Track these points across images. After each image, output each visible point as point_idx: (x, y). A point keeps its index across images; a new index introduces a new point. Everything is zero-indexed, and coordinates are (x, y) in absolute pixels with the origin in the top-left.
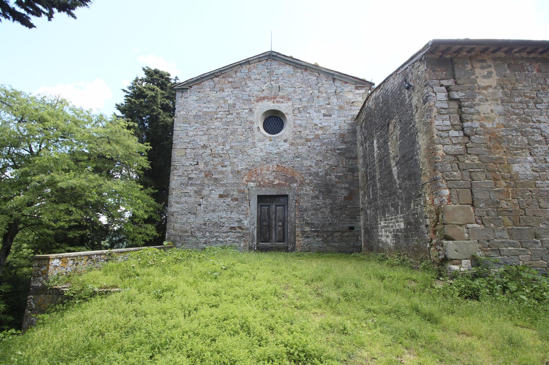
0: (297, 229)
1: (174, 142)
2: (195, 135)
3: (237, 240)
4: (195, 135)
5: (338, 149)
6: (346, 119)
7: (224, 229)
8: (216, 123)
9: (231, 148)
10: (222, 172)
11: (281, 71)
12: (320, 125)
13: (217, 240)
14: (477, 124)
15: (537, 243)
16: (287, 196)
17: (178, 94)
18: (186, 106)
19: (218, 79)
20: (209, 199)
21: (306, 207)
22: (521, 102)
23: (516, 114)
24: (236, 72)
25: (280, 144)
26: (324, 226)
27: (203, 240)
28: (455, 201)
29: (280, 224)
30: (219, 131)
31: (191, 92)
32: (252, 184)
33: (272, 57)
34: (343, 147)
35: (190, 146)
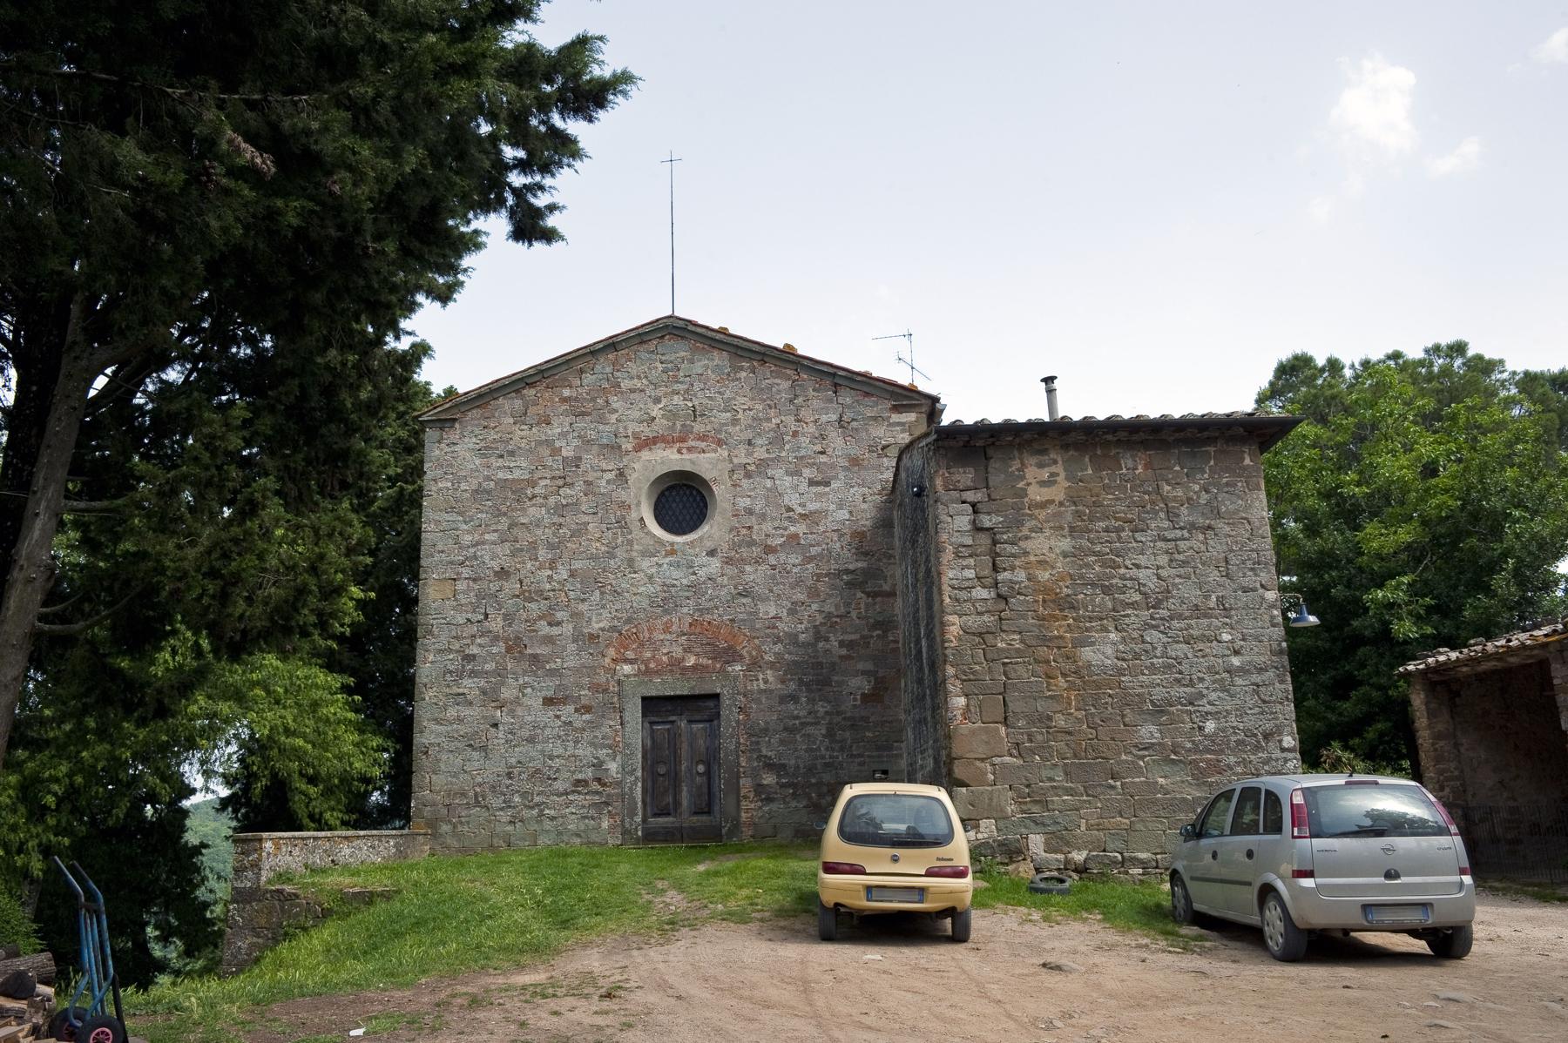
0: (742, 782)
1: (423, 562)
2: (477, 544)
3: (592, 812)
4: (477, 544)
5: (847, 572)
6: (866, 490)
7: (560, 786)
8: (532, 511)
9: (573, 574)
10: (549, 640)
11: (698, 368)
12: (800, 510)
13: (541, 814)
14: (1021, 575)
15: (1113, 787)
16: (716, 696)
17: (430, 435)
18: (452, 466)
19: (533, 392)
20: (519, 711)
21: (767, 723)
22: (1107, 530)
23: (1095, 554)
24: (582, 371)
25: (698, 561)
26: (811, 770)
27: (504, 817)
28: (975, 717)
29: (701, 768)
30: (539, 532)
31: (463, 428)
32: (627, 669)
33: (673, 330)
34: (860, 565)
35: (466, 572)
